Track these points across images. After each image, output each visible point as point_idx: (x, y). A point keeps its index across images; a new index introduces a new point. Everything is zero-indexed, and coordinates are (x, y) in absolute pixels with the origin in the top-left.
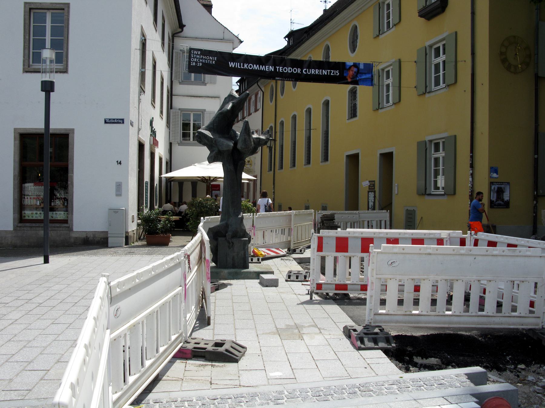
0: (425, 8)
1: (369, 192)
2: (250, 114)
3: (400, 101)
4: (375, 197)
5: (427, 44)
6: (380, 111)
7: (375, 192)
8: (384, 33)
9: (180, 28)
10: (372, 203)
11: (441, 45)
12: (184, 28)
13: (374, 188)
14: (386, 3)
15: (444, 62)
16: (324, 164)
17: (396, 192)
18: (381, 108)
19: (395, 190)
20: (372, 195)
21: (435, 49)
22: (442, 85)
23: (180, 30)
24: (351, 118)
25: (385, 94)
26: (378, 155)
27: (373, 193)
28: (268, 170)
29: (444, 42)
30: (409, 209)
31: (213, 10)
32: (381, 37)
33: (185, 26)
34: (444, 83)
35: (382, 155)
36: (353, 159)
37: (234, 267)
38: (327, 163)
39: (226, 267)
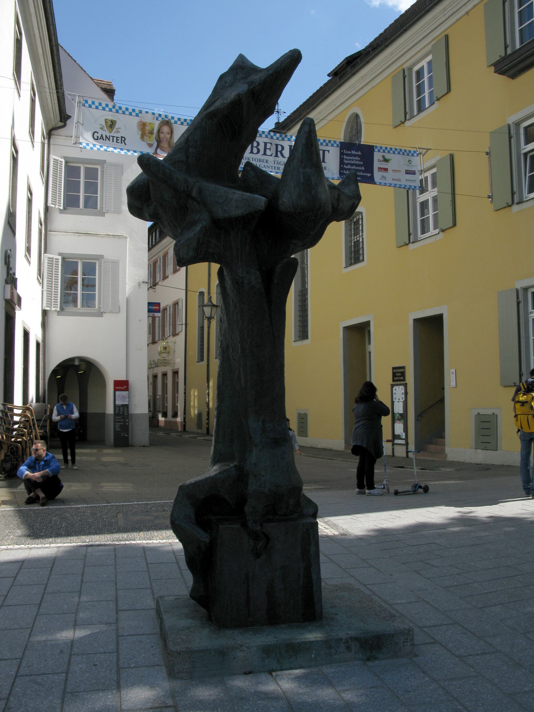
0: (502, 60)
1: (392, 386)
2: (165, 277)
3: (455, 225)
4: (406, 393)
5: (511, 120)
6: (411, 246)
7: (405, 385)
8: (412, 117)
9: (61, 121)
10: (401, 404)
11: (428, 174)
12: (68, 122)
13: (404, 380)
14: (416, 68)
15: (435, 199)
16: (300, 343)
17: (453, 384)
18: (413, 242)
19: (450, 379)
20: (399, 391)
21: (526, 128)
22: (432, 231)
23: (61, 124)
24: (351, 264)
25: (419, 219)
26: (411, 322)
27: (402, 387)
28: (293, 339)
29: (434, 170)
30: (482, 412)
31: (115, 97)
32: (407, 123)
33: (69, 117)
34: (435, 228)
35: (418, 322)
36: (358, 333)
37: (273, 619)
38: (305, 342)
39: (245, 621)
